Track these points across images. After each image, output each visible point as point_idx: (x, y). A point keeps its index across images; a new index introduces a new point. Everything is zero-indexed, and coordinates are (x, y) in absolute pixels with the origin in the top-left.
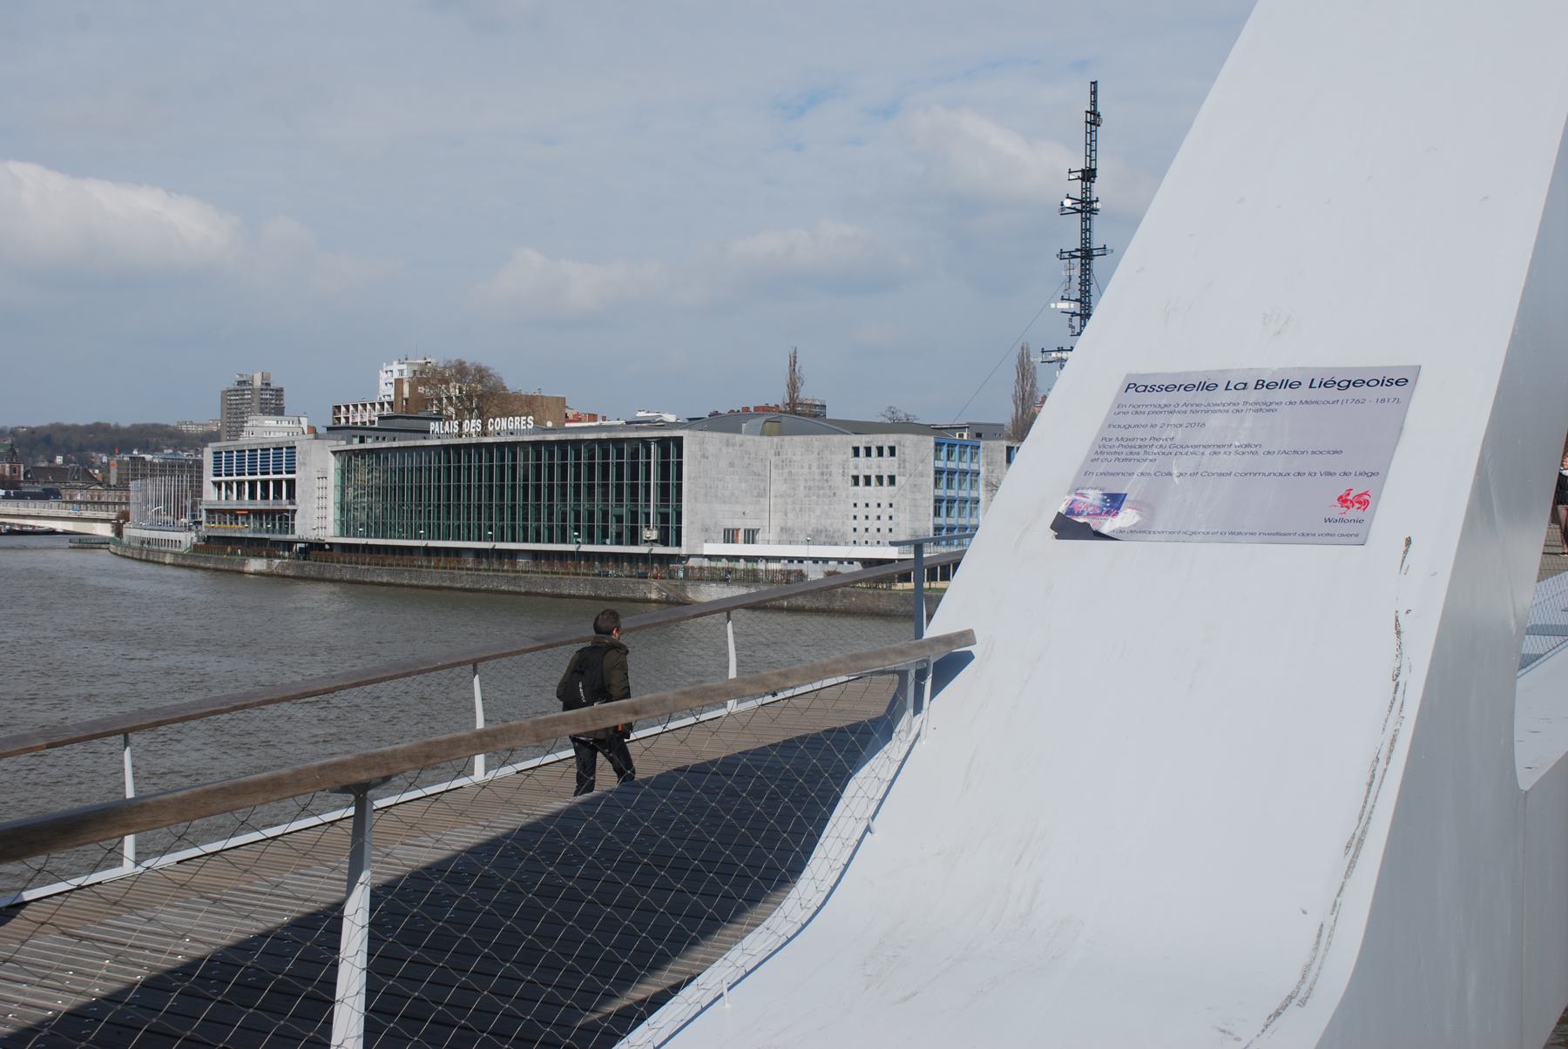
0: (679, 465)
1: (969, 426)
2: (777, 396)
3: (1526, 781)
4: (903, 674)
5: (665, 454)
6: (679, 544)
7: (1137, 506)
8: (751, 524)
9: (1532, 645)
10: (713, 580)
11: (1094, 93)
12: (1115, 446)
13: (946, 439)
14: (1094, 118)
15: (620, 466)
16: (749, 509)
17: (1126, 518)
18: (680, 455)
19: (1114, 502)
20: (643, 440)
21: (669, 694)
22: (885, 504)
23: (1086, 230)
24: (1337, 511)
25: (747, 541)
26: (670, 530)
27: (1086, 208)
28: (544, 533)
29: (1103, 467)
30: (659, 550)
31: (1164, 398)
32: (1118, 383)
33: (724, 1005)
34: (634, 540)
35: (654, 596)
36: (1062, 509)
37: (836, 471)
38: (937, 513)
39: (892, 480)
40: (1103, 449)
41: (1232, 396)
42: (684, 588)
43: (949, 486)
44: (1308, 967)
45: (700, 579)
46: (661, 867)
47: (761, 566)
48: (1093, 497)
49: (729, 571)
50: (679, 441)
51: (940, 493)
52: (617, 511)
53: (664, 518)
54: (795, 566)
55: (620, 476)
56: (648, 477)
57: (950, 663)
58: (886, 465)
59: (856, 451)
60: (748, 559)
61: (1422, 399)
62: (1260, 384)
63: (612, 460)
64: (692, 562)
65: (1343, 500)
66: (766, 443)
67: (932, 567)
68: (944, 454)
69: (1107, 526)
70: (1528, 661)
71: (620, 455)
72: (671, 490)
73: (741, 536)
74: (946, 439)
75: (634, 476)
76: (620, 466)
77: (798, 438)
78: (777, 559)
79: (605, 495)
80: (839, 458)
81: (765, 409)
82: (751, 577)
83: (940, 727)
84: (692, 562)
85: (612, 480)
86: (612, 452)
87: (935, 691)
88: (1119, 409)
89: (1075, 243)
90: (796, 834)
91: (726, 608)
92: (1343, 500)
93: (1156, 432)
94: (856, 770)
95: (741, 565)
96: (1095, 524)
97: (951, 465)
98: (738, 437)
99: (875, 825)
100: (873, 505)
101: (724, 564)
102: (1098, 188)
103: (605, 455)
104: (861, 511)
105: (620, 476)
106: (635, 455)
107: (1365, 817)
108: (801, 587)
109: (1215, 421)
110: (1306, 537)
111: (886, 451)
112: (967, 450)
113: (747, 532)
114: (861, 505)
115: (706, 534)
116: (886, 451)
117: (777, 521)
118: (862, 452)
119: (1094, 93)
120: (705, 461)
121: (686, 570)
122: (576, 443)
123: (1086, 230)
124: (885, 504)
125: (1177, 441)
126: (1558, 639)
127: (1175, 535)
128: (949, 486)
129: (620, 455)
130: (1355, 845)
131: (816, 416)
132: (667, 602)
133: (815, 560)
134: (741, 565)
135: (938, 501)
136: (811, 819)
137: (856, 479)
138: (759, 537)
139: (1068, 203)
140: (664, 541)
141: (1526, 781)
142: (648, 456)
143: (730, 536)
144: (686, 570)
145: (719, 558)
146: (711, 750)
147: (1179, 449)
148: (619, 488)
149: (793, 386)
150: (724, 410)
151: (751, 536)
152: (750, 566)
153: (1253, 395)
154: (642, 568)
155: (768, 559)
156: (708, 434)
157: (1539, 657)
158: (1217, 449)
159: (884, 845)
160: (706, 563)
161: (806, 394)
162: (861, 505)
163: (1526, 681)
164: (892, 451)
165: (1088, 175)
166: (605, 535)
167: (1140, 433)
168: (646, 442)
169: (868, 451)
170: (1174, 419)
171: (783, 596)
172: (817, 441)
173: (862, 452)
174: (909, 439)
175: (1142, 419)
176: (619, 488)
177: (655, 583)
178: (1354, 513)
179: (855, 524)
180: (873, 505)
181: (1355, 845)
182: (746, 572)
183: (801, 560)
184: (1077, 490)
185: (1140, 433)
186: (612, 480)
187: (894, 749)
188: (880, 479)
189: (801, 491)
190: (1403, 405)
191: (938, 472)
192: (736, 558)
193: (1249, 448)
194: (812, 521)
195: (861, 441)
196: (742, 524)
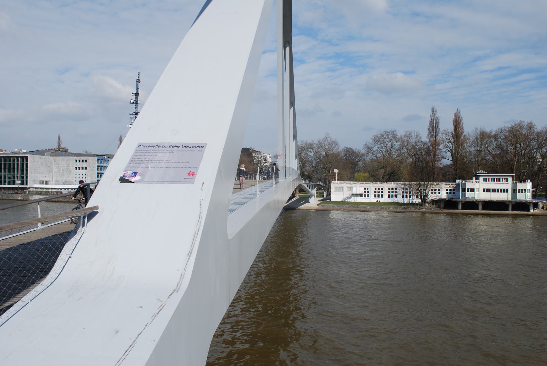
0: (27, 164)
1: (106, 155)
2: (55, 146)
3: (230, 237)
4: (79, 217)
5: (23, 161)
6: (27, 184)
7: (140, 175)
8: (47, 180)
9: (232, 207)
10: (36, 194)
11: (139, 75)
12: (135, 160)
13: (100, 158)
14: (139, 81)
15: (10, 164)
16: (48, 175)
17: (138, 178)
18: (27, 161)
19: (135, 174)
20: (17, 157)
21: (11, 224)
22: (84, 174)
23: (136, 108)
24: (187, 176)
25: (46, 184)
26: (24, 181)
27: (136, 102)
28: (11, 182)
29: (132, 165)
30: (21, 186)
31: (147, 149)
32: (137, 145)
33: (29, 305)
34: (14, 184)
35: (20, 198)
36: (122, 175)
37: (71, 166)
38: (98, 177)
39: (86, 168)
40: (132, 161)
41: (164, 149)
42: (28, 196)
43: (101, 170)
44: (179, 283)
45: (33, 194)
46: (10, 270)
47: (50, 190)
48: (130, 173)
49: (41, 192)
50: (27, 157)
51: (99, 172)
52: (9, 176)
53: (23, 178)
54: (60, 190)
55: (10, 166)
56: (18, 167)
57: (92, 215)
58: (84, 165)
59: (76, 161)
60: (46, 188)
61: (207, 150)
62: (170, 146)
63: (7, 162)
64: (31, 189)
65: (189, 174)
66: (52, 158)
67: (85, 191)
68: (100, 162)
69: (133, 180)
70: (231, 211)
71: (10, 161)
72: (24, 170)
73: (45, 182)
74: (100, 158)
75: (14, 166)
76: (10, 164)
77: (60, 157)
78: (55, 189)
79: (5, 172)
80: (72, 162)
81: (52, 149)
82: (47, 193)
83: (89, 231)
84: (31, 189)
85: (7, 167)
86: (7, 160)
87: (88, 221)
88: (136, 151)
89: (133, 111)
90: (49, 259)
91: (38, 201)
92: (189, 174)
93: (145, 157)
94: (66, 242)
95: (45, 190)
96: (130, 179)
97: (102, 165)
98: (44, 157)
99: (71, 256)
100: (81, 175)
101: (40, 190)
102: (139, 98)
103: (5, 161)
104: (77, 176)
105: (10, 166)
106: (14, 161)
107: (192, 247)
108: (59, 195)
109: (160, 155)
110: (180, 182)
111: (84, 161)
112: (104, 159)
113: (46, 181)
114: (78, 175)
115: (35, 182)
116: (84, 161)
117: (55, 179)
118: (78, 161)
119: (139, 75)
120: (34, 164)
121: (29, 191)
122: (9, 157)
123: (136, 108)
124: (84, 174)
125: (151, 159)
126: (239, 205)
127: (149, 182)
128: (101, 170)
129: (10, 161)
130: (190, 254)
131: (65, 152)
132: (23, 200)
133: (65, 189)
134: (45, 190)
135: (98, 174)
136: (53, 255)
137: (76, 168)
138: (49, 183)
139: (132, 101)
140: (23, 184)
141: (230, 237)
142: (18, 161)
143: (41, 182)
144: (29, 191)
145: (38, 188)
146: (34, 238)
147: (151, 161)
148: (9, 170)
149: (59, 144)
150: (40, 150)
151: (47, 183)
152: (47, 190)
153: (169, 149)
154: (16, 191)
155: (52, 188)
156: (35, 156)
157: (44, 201)
158: (160, 161)
159: (74, 262)
160: (35, 190)
161: (63, 146)
162: (78, 175)
163: (231, 216)
164: (86, 161)
165: (137, 94)
166: (5, 182)
167: (141, 157)
168: (17, 158)
169: (80, 161)
170: (150, 154)
171: (54, 198)
172: (66, 158)
173: (78, 161)
174: (91, 158)
175: (142, 154)
176: (9, 170)
177: (20, 195)
178: (191, 177)
179: (76, 179)
180: (81, 175)
181: (190, 254)
182: (46, 192)
183: (61, 189)
184: (126, 171)
185: (141, 157)
186: (7, 167)
187: (77, 236)
188: (79, 168)
189: (61, 171)
190: (203, 152)
191: (98, 166)
192: (43, 188)
193: (167, 161)
194: (64, 179)
195: (78, 158)
196: (45, 180)
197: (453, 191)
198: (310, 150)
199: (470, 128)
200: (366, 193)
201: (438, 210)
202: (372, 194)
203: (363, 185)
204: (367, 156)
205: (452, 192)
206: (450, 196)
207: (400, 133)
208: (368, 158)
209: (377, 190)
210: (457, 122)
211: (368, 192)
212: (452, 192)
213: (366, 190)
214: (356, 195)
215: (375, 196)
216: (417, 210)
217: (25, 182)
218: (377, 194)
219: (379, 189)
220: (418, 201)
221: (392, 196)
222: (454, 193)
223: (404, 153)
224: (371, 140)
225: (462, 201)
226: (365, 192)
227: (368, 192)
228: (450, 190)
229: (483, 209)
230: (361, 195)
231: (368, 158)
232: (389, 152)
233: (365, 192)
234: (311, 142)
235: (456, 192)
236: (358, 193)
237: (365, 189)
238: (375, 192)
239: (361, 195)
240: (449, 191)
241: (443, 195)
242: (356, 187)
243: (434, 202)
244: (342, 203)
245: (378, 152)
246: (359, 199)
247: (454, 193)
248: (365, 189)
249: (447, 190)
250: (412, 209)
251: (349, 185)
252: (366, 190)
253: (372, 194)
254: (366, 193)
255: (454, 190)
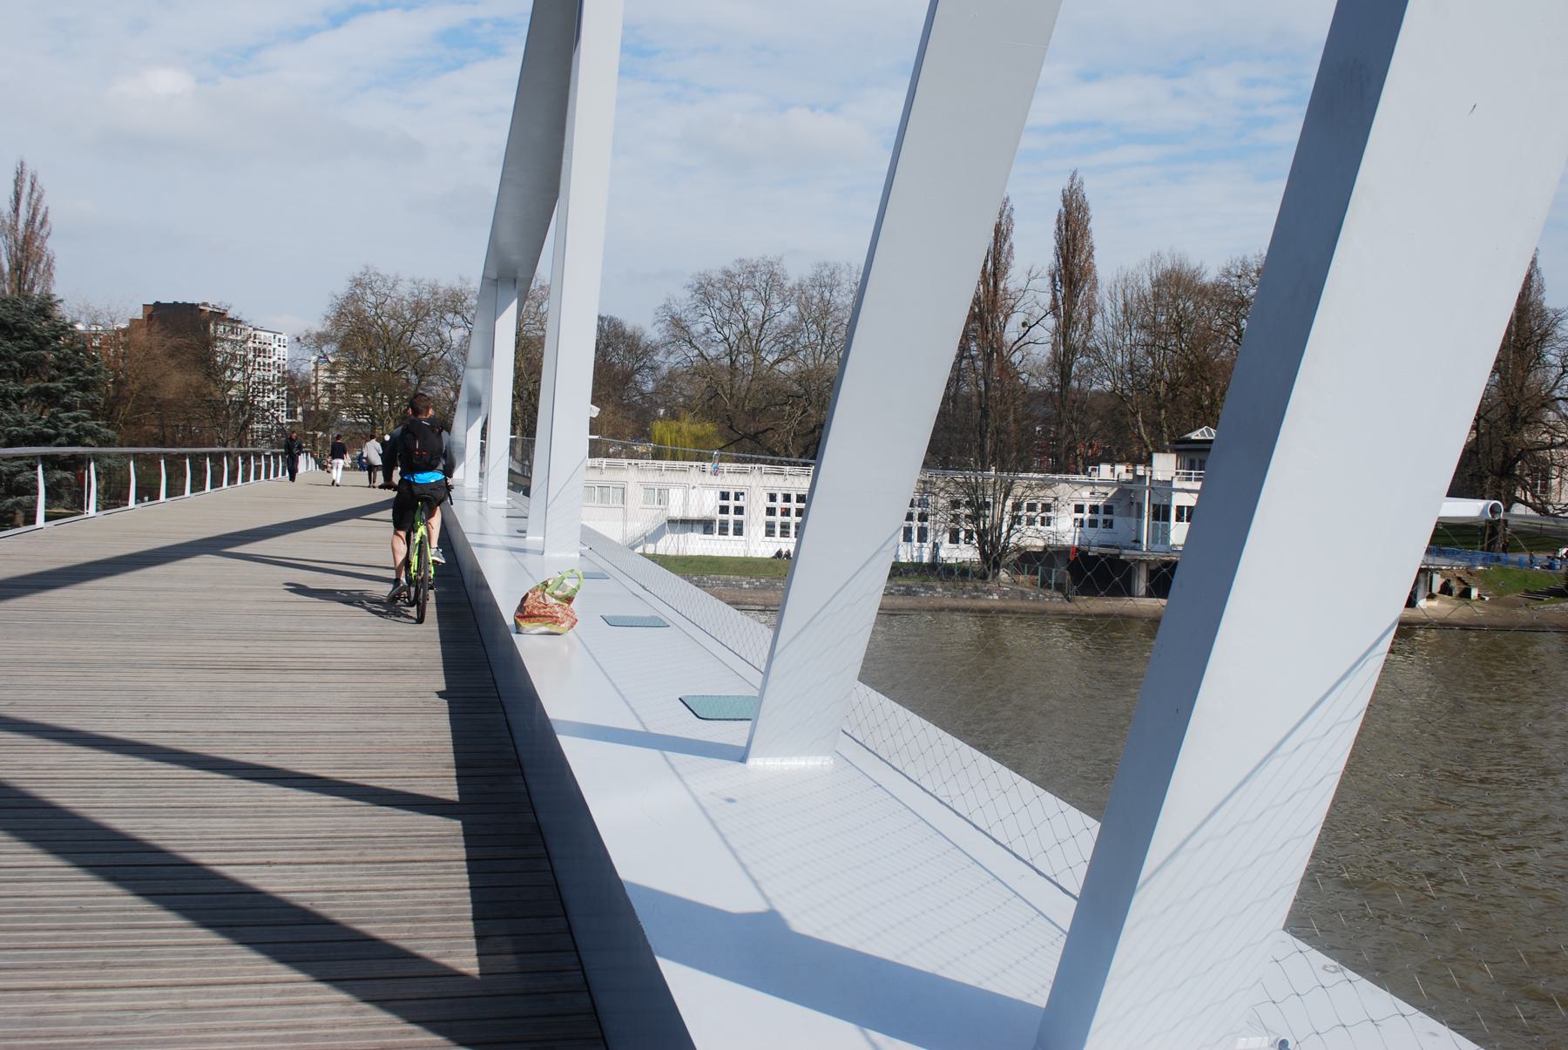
8: (766, 498)
197: (1103, 515)
198: (449, 317)
201: (1054, 602)
202: (756, 520)
203: (717, 480)
204: (670, 353)
205: (1101, 517)
206: (1091, 533)
207: (796, 272)
208: (667, 361)
209: (779, 504)
211: (739, 510)
212: (1101, 517)
213: (732, 503)
214: (686, 524)
215: (770, 531)
216: (964, 601)
217: (811, 452)
218: (778, 519)
219: (787, 498)
220: (967, 553)
221: (785, 526)
222: (1109, 524)
223: (231, 384)
224: (688, 293)
225: (1148, 563)
226: (724, 510)
227: (739, 510)
228: (1094, 509)
229: (1149, 594)
230: (706, 526)
231: (672, 359)
232: (749, 340)
233: (724, 510)
234: (457, 285)
235: (1118, 521)
236: (693, 514)
237: (725, 496)
238: (771, 511)
239: (706, 526)
240: (1086, 516)
241: (1065, 529)
242: (685, 487)
243: (1028, 560)
245: (712, 338)
247: (1109, 524)
248: (725, 496)
249: (1079, 509)
250: (941, 594)
251: (652, 478)
252: (732, 503)
253: (756, 520)
255: (1108, 509)
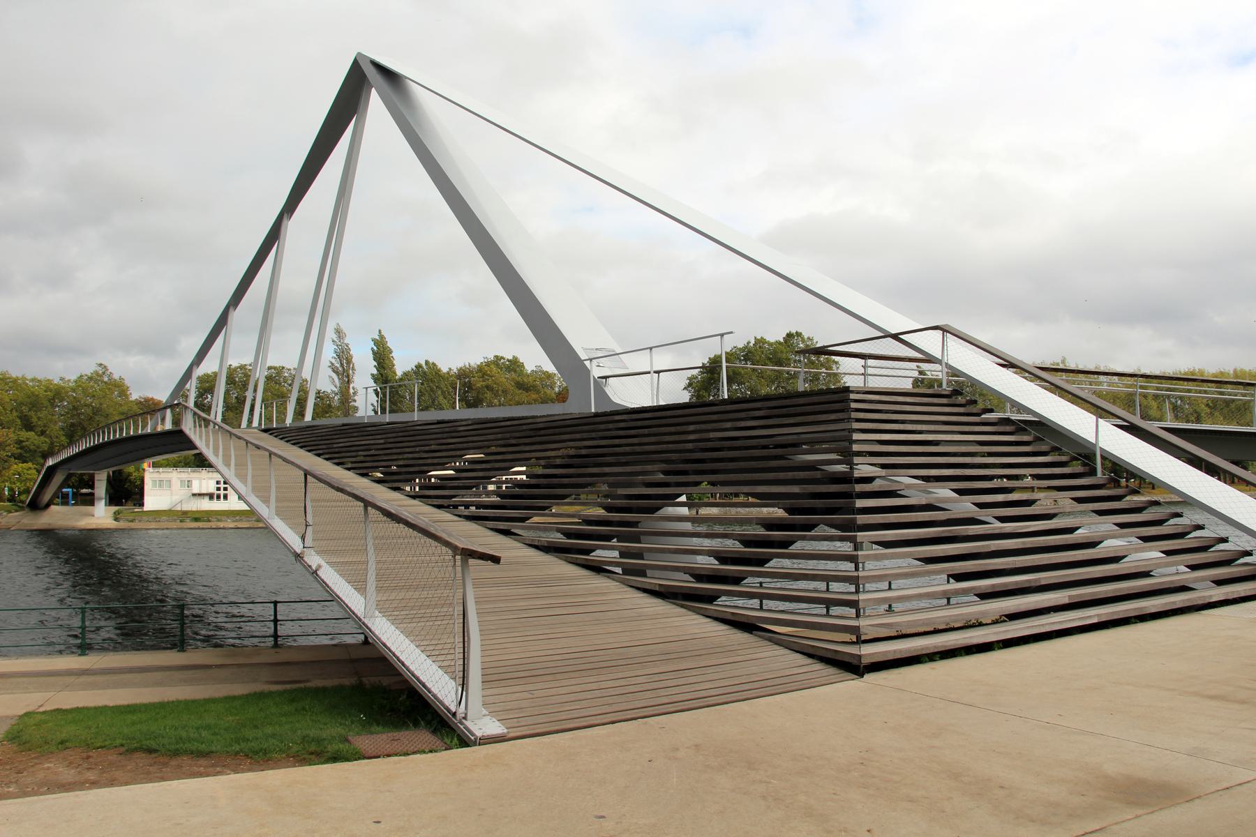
2: (472, 561)
199: (403, 364)
200: (222, 492)
210: (382, 356)
226: (218, 489)
230: (211, 496)
236: (204, 491)
239: (211, 496)
242: (200, 479)
244: (169, 514)
246: (206, 505)
254: (222, 492)
